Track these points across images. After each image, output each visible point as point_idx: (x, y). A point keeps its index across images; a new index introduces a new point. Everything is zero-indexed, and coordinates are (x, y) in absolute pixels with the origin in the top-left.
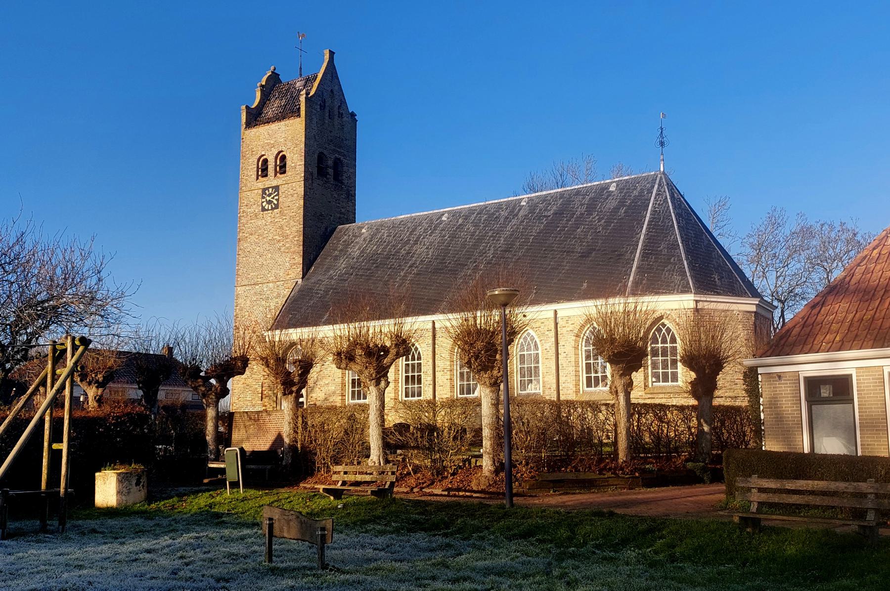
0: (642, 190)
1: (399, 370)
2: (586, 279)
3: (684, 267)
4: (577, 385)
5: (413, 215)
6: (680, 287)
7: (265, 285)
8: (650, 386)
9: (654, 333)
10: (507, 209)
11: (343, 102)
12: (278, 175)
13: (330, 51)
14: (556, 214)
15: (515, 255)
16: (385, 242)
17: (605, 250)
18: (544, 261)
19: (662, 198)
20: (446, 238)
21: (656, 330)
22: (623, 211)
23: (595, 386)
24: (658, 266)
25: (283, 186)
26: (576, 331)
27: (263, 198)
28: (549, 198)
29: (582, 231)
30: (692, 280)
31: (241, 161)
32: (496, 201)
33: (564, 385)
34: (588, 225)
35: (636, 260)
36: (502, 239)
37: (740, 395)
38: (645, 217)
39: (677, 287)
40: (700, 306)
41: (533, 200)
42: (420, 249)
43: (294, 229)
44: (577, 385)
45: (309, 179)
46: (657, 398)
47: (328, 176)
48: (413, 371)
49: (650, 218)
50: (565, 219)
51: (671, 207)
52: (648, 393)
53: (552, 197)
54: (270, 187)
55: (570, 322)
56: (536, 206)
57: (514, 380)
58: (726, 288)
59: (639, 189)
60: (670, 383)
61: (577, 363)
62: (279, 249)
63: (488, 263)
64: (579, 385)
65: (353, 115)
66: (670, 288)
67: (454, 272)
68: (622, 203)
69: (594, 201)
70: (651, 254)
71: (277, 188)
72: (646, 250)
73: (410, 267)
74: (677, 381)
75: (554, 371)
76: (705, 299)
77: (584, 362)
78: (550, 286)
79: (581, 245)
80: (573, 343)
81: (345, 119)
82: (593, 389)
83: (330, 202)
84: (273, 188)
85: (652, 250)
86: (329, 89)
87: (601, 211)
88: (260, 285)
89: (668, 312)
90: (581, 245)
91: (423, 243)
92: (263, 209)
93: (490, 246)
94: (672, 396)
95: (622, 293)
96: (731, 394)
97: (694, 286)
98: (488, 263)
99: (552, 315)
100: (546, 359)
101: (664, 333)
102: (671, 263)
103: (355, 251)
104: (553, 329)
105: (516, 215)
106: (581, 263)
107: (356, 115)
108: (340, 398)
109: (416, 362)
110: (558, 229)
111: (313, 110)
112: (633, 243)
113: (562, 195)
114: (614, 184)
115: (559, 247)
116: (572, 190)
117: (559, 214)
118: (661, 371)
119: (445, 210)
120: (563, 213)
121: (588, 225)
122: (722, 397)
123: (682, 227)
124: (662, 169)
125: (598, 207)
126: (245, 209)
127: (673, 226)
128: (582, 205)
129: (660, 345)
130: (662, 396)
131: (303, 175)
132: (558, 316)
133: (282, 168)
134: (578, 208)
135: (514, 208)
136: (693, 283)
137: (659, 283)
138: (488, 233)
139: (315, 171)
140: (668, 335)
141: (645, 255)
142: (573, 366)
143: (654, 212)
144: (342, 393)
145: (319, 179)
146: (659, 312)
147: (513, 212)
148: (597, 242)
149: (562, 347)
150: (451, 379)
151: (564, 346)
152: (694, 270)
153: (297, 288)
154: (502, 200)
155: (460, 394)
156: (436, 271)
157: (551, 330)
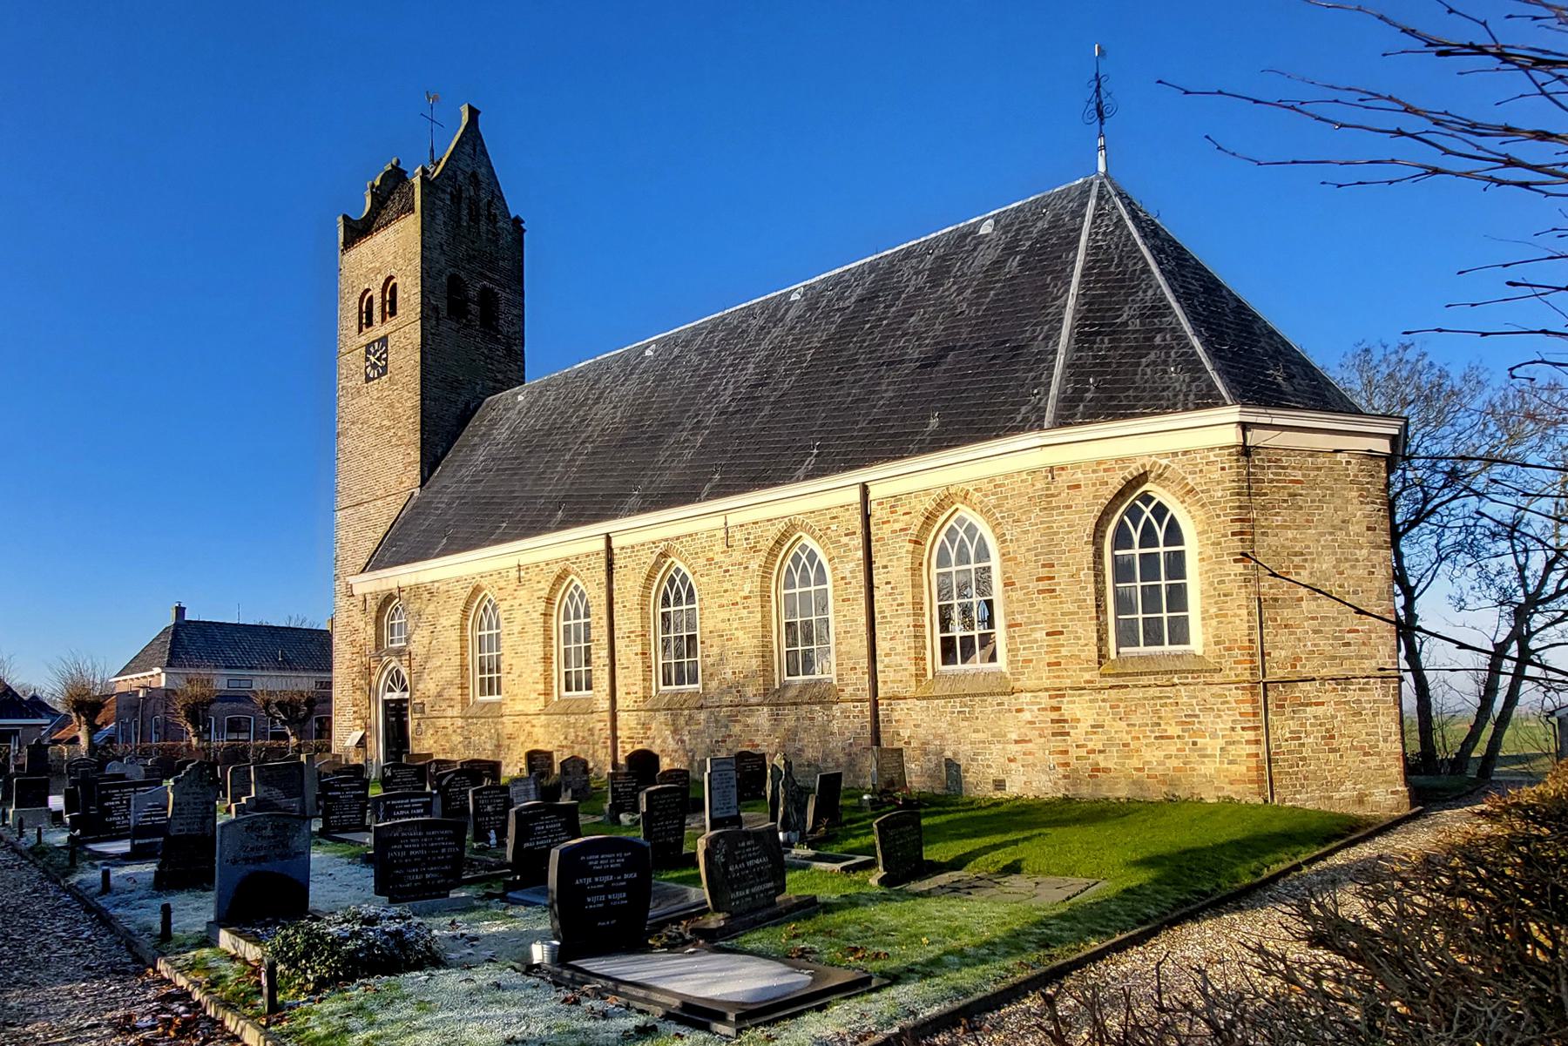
0: (1057, 217)
1: (551, 639)
2: (937, 409)
3: (1195, 353)
4: (1102, 639)
5: (599, 358)
6: (1192, 397)
7: (371, 505)
8: (1113, 655)
9: (1121, 523)
10: (762, 313)
11: (497, 196)
12: (388, 319)
13: (469, 106)
14: (862, 300)
15: (775, 390)
16: (549, 410)
17: (977, 345)
18: (838, 390)
19: (1111, 219)
20: (649, 383)
21: (1126, 513)
22: (1015, 264)
23: (964, 660)
24: (1123, 356)
25: (393, 335)
26: (914, 530)
27: (367, 359)
28: (847, 277)
29: (921, 320)
30: (1221, 378)
31: (339, 306)
32: (744, 305)
33: (887, 660)
34: (934, 305)
35: (1061, 349)
36: (751, 366)
37: (1357, 673)
38: (1074, 262)
39: (1181, 397)
40: (1255, 437)
41: (814, 288)
42: (603, 411)
43: (409, 404)
44: (1102, 639)
45: (429, 314)
46: (1136, 686)
47: (469, 317)
48: (577, 640)
49: (1086, 262)
50: (882, 306)
51: (1136, 234)
52: (1110, 675)
53: (853, 274)
54: (374, 342)
55: (900, 510)
56: (821, 294)
57: (772, 651)
58: (1311, 399)
59: (1049, 216)
60: (1167, 648)
61: (918, 605)
62: (389, 442)
63: (721, 413)
64: (924, 659)
65: (518, 222)
66: (1164, 403)
67: (656, 440)
68: (1010, 249)
69: (945, 261)
70: (1098, 333)
71: (384, 340)
72: (1086, 326)
73: (581, 444)
74: (1186, 641)
75: (863, 629)
76: (1267, 420)
77: (936, 604)
78: (852, 437)
79: (919, 346)
80: (908, 560)
81: (500, 224)
82: (959, 667)
83: (474, 361)
84: (378, 340)
85: (1101, 326)
86: (469, 171)
87: (964, 275)
88: (366, 505)
89: (1164, 462)
90: (919, 346)
91: (608, 401)
92: (368, 379)
93: (727, 383)
94: (1176, 680)
95: (1034, 423)
96: (1334, 671)
97: (1230, 392)
98: (721, 413)
99: (854, 496)
100: (843, 601)
101: (1148, 518)
102: (1154, 347)
103: (501, 433)
104: (859, 531)
105: (781, 320)
106: (921, 380)
107: (523, 222)
108: (459, 691)
109: (583, 620)
110: (868, 326)
111: (437, 202)
112: (1049, 318)
113: (873, 267)
114: (991, 221)
115: (869, 359)
116: (896, 252)
117: (869, 299)
118: (1165, 615)
119: (649, 345)
120: (878, 296)
121: (934, 305)
122: (1314, 679)
123: (1170, 272)
124: (1102, 168)
125: (956, 269)
126: (345, 384)
127: (1146, 269)
128: (917, 273)
129: (1137, 551)
130: (1151, 680)
131: (419, 310)
132: (871, 497)
133: (391, 308)
134: (909, 280)
135: (777, 308)
136: (1226, 385)
137: (1131, 393)
138: (725, 360)
139: (443, 305)
140: (1136, 529)
141: (1082, 338)
142: (908, 615)
143: (1094, 249)
144: (462, 684)
145: (451, 319)
146: (1138, 464)
147: (775, 315)
148: (958, 333)
149: (881, 570)
150: (643, 654)
151: (885, 567)
152: (1220, 358)
153: (413, 502)
154: (754, 301)
155: (664, 684)
156: (624, 444)
157: (854, 533)
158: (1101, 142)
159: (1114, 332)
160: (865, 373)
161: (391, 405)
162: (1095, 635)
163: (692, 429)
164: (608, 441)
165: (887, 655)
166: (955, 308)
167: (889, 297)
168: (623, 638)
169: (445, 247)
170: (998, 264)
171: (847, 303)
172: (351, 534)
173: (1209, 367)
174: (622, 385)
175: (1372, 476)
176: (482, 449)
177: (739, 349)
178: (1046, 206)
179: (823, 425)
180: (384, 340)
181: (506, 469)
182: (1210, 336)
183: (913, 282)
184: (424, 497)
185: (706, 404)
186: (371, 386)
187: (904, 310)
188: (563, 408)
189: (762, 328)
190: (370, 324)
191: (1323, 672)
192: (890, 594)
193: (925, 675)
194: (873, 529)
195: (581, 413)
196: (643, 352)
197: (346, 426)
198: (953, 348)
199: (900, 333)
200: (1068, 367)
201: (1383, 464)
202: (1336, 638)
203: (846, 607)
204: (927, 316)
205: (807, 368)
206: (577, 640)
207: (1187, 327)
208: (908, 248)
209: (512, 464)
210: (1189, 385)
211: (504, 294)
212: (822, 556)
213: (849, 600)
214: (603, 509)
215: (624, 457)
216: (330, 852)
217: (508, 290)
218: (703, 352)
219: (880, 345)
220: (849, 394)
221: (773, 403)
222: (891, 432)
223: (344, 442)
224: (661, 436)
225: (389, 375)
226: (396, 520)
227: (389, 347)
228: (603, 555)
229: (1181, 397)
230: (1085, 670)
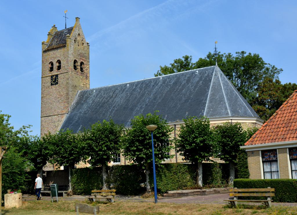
42: (117, 100)
54: (54, 75)
71: (57, 76)
92: (52, 85)
117: (175, 83)
141: (211, 102)
170: (198, 82)
171: (171, 84)
176: (85, 105)
177: (149, 89)
180: (57, 76)
197: (45, 95)
200: (208, 108)
216: (74, 198)
217: (86, 61)
225: (58, 84)
227: (58, 78)
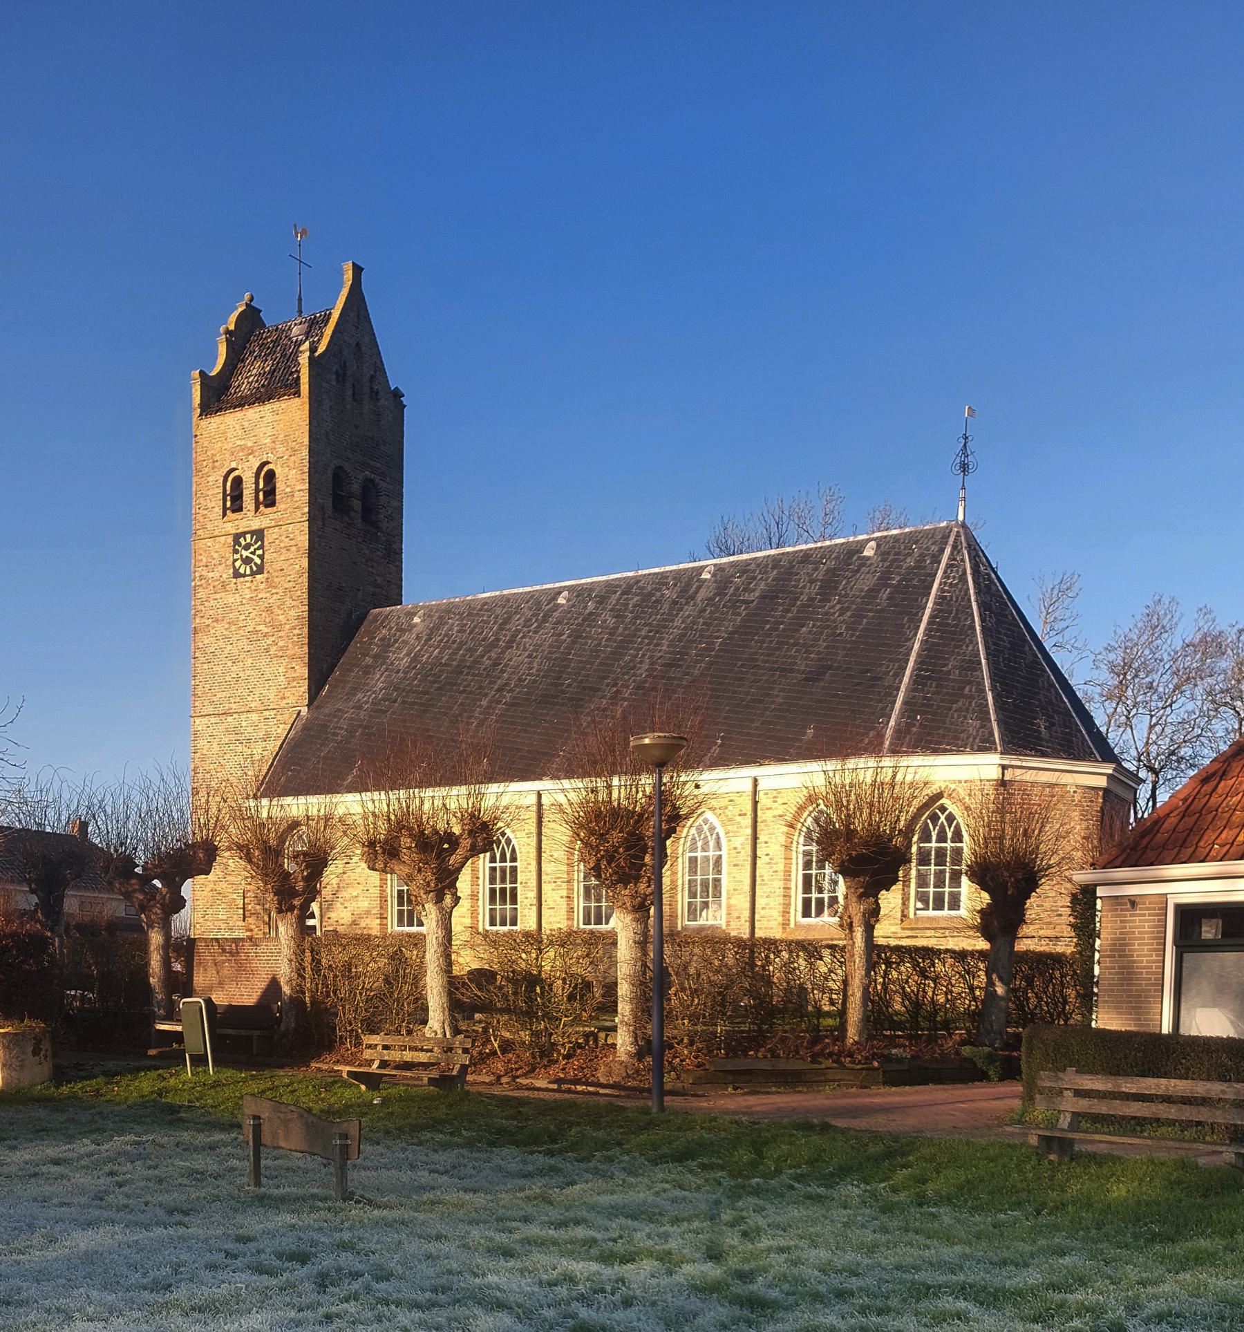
1: (478, 878)
4: (786, 913)
5: (506, 592)
7: (244, 716)
10: (675, 585)
11: (379, 368)
12: (262, 508)
13: (353, 263)
15: (687, 674)
16: (454, 642)
19: (957, 571)
20: (564, 637)
22: (885, 596)
23: (818, 914)
25: (271, 531)
28: (753, 567)
29: (810, 632)
30: (999, 727)
31: (194, 479)
33: (763, 912)
35: (903, 688)
39: (971, 739)
42: (516, 657)
43: (292, 613)
44: (786, 913)
48: (503, 880)
49: (933, 611)
50: (781, 608)
52: (908, 929)
53: (758, 565)
54: (245, 533)
55: (780, 801)
65: (397, 394)
66: (960, 742)
68: (884, 579)
71: (259, 534)
76: (1019, 763)
80: (782, 839)
84: (252, 533)
87: (846, 595)
88: (235, 716)
89: (953, 786)
90: (806, 659)
92: (237, 574)
93: (643, 655)
94: (947, 934)
95: (874, 749)
96: (1049, 933)
102: (963, 696)
108: (378, 921)
109: (508, 864)
110: (768, 626)
113: (776, 561)
114: (873, 544)
115: (767, 661)
117: (769, 598)
120: (777, 597)
124: (961, 517)
126: (203, 573)
127: (973, 627)
128: (812, 582)
129: (934, 844)
133: (268, 497)
134: (804, 587)
137: (941, 731)
138: (640, 630)
143: (941, 599)
151: (766, 843)
157: (745, 815)
158: (962, 494)
159: (940, 679)
160: (763, 674)
161: (269, 610)
162: (900, 901)
163: (611, 698)
164: (527, 693)
165: (763, 908)
166: (836, 628)
167: (787, 601)
168: (549, 882)
169: (331, 437)
170: (873, 592)
172: (215, 745)
173: (993, 717)
174: (536, 632)
175: (1092, 801)
178: (916, 542)
179: (726, 718)
181: (414, 703)
182: (1003, 690)
183: (807, 590)
184: (316, 719)
185: (623, 674)
186: (241, 583)
187: (799, 618)
188: (470, 644)
189: (675, 603)
190: (238, 508)
191: (1041, 933)
192: (769, 863)
193: (789, 925)
194: (759, 813)
195: (493, 655)
196: (555, 598)
198: (830, 668)
199: (792, 641)
201: (1101, 793)
202: (1052, 911)
203: (735, 870)
204: (815, 629)
205: (716, 657)
206: (503, 880)
207: (987, 682)
208: (807, 550)
209: (421, 698)
210: (977, 731)
211: (384, 485)
212: (720, 830)
213: (737, 865)
214: (530, 765)
215: (547, 715)
217: (388, 480)
218: (619, 616)
219: (777, 649)
220: (748, 693)
221: (685, 687)
222: (779, 735)
223: (204, 640)
224: (582, 699)
226: (284, 740)
227: (266, 543)
228: (534, 808)
229: (971, 739)
230: (892, 924)
